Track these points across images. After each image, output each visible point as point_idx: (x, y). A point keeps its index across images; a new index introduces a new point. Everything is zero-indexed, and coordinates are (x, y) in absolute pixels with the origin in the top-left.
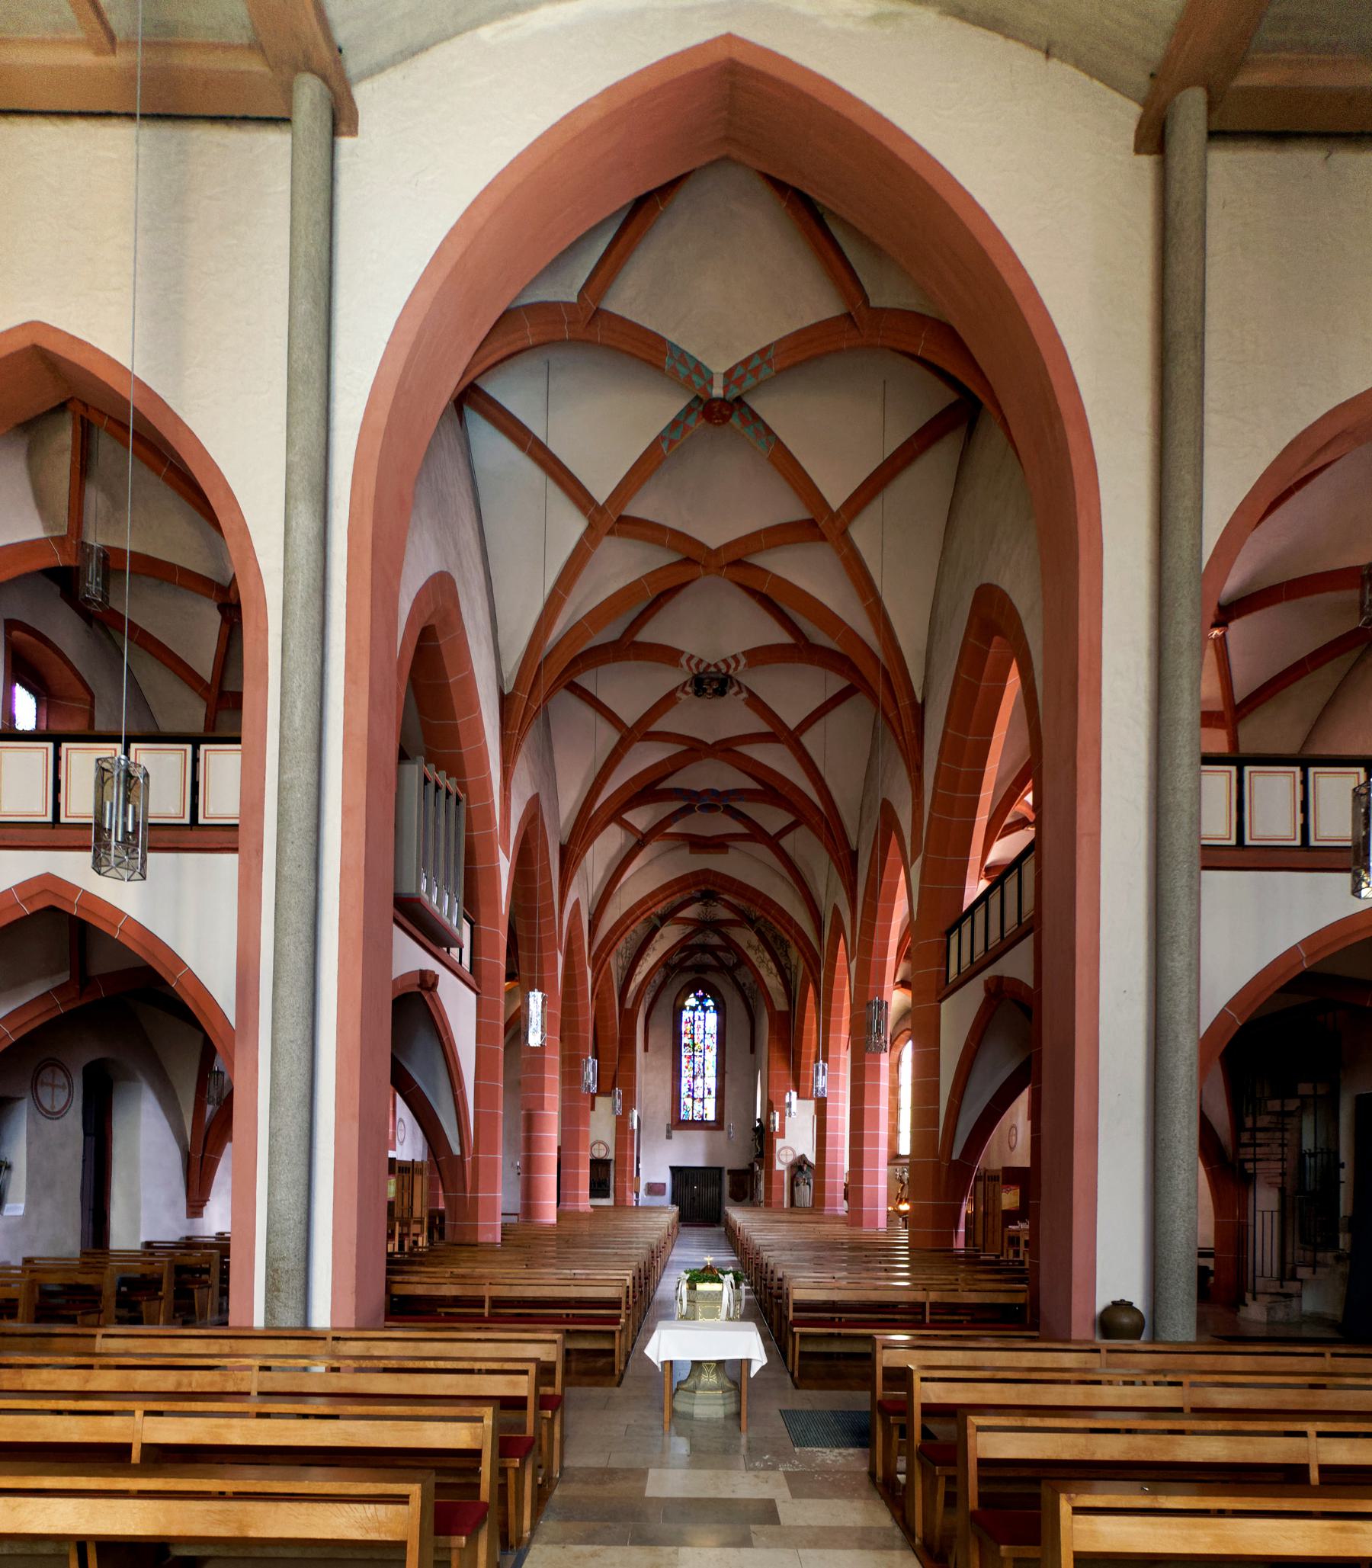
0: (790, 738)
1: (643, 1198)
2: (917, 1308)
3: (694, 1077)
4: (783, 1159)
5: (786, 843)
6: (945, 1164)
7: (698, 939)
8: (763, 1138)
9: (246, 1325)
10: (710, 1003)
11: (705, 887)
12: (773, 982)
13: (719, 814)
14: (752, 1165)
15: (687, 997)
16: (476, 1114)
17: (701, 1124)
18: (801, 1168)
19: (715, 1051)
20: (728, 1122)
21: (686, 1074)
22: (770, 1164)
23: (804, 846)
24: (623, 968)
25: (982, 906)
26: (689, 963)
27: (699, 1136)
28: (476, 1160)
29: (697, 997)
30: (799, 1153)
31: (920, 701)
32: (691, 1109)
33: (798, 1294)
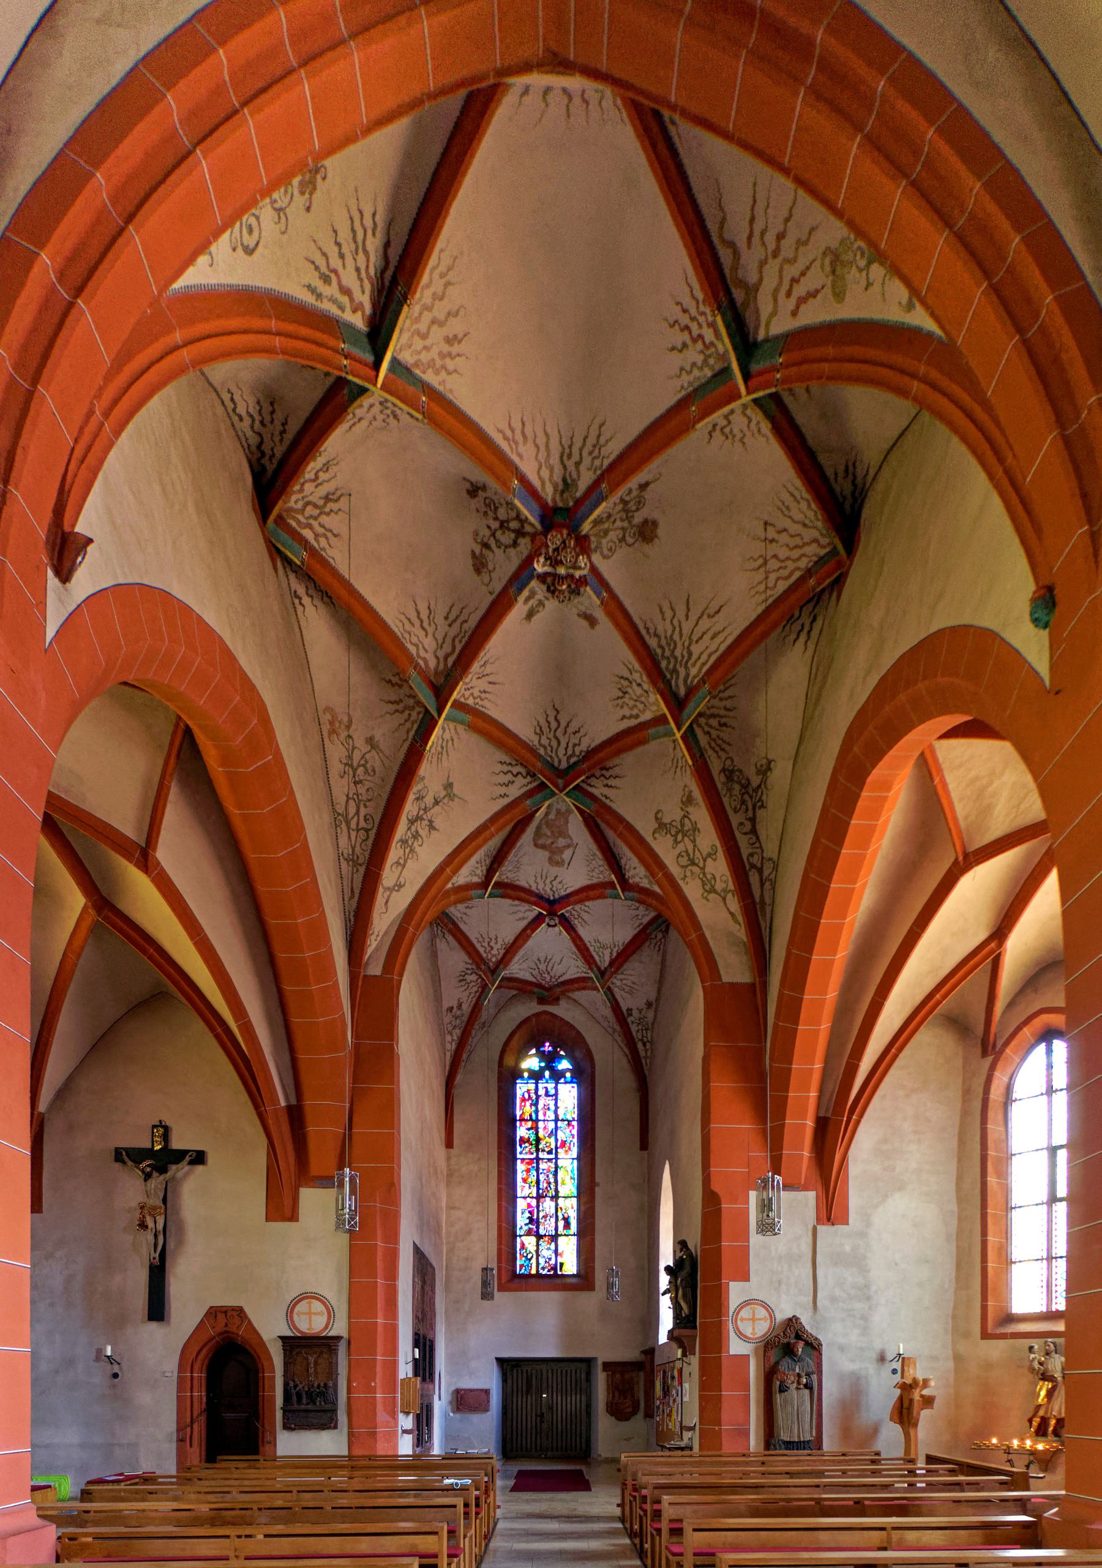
3: (539, 1197)
9: (390, 1453)
10: (564, 1065)
15: (522, 1054)
17: (553, 1279)
18: (788, 1351)
19: (574, 1152)
21: (524, 1190)
22: (715, 1340)
29: (542, 1055)
30: (781, 1316)
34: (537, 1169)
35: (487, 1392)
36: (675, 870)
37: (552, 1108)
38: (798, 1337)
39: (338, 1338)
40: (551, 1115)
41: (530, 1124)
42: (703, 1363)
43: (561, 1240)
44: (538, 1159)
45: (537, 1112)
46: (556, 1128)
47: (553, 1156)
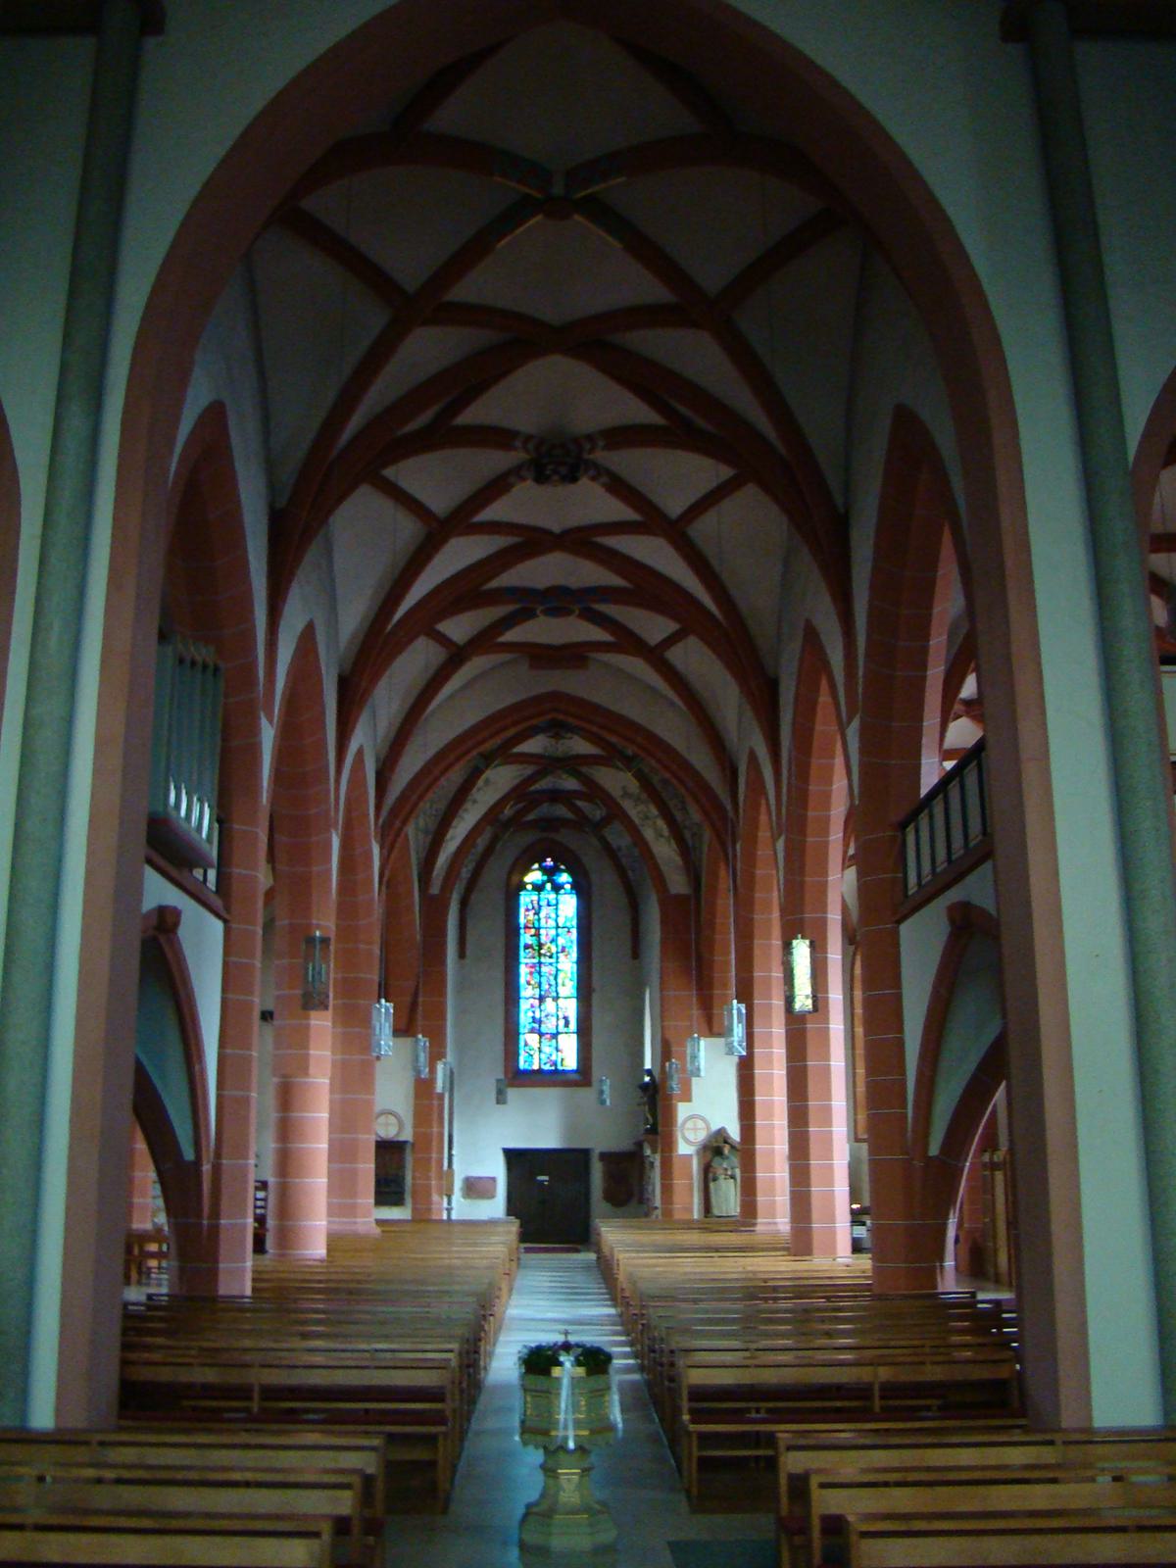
0: (676, 531)
1: (461, 1207)
2: (862, 1392)
3: (541, 999)
4: (691, 1136)
5: (703, 529)
6: (918, 1163)
7: (544, 784)
8: (655, 1101)
10: (564, 878)
11: (555, 714)
12: (665, 851)
13: (572, 619)
14: (640, 1145)
15: (527, 870)
16: (219, 1097)
17: (550, 1077)
18: (718, 1152)
20: (597, 1072)
21: (527, 992)
22: (669, 1144)
23: (695, 658)
24: (426, 832)
25: (955, 782)
26: (531, 817)
27: (551, 1099)
28: (217, 1169)
29: (546, 871)
30: (715, 1127)
31: (842, 510)
32: (533, 1054)
33: (696, 1377)
34: (539, 973)
35: (493, 1179)
36: (637, 821)
37: (553, 916)
38: (726, 1142)
39: (405, 1142)
40: (552, 923)
41: (533, 931)
42: (662, 1158)
43: (560, 1037)
44: (540, 963)
45: (539, 920)
46: (557, 935)
47: (553, 960)
